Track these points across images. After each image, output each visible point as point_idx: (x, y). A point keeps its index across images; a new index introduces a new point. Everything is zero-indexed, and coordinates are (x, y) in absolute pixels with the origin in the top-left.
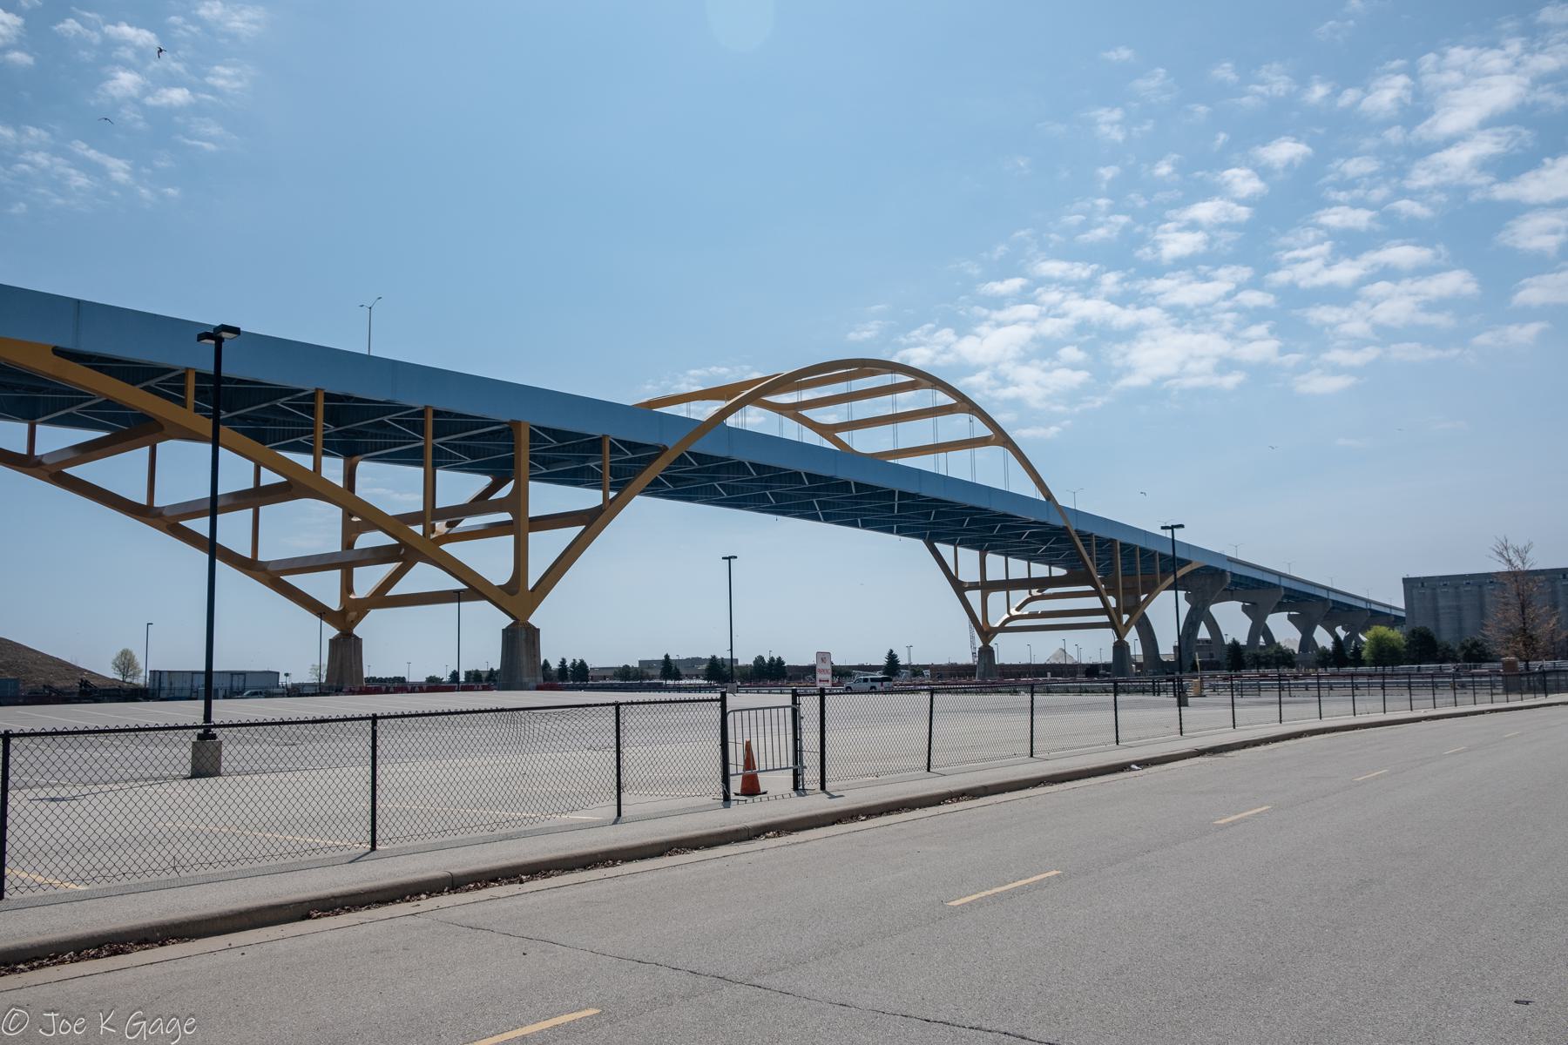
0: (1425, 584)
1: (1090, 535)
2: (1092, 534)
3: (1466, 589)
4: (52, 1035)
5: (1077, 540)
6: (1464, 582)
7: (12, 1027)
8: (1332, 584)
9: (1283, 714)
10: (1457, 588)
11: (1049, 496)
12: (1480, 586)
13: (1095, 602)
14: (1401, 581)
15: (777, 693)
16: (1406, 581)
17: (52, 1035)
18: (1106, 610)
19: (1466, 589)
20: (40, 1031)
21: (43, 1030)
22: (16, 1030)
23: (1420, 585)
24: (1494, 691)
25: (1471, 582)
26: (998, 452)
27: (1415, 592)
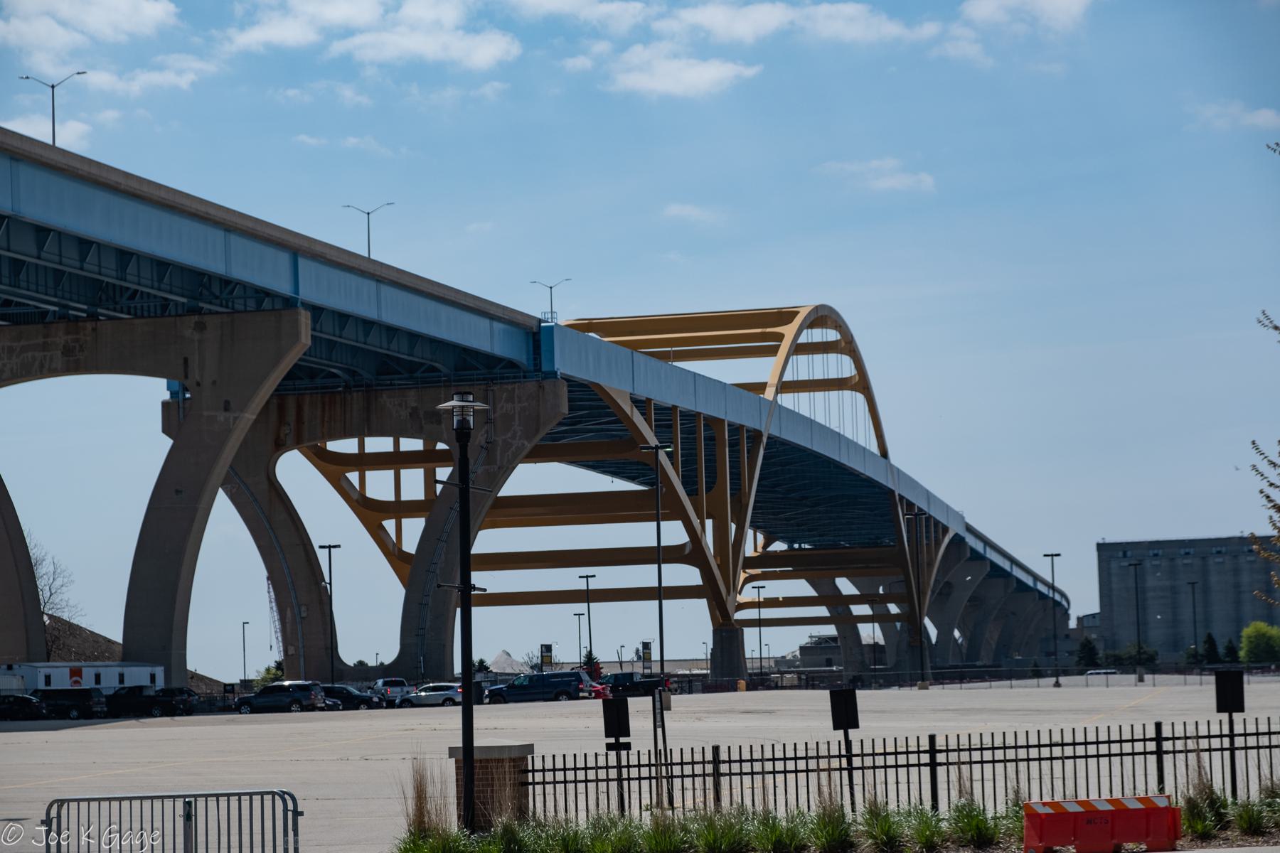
0: (1129, 553)
1: (649, 400)
2: (675, 407)
3: (1186, 561)
4: (41, 845)
5: (638, 419)
6: (1182, 551)
7: (10, 838)
8: (696, 408)
9: (1123, 733)
10: (1172, 559)
11: (884, 454)
12: (1203, 558)
13: (674, 534)
14: (1095, 548)
15: (986, 688)
16: (1102, 548)
17: (41, 845)
18: (691, 554)
19: (1186, 561)
20: (33, 841)
21: (36, 841)
22: (13, 841)
23: (1121, 554)
24: (530, 768)
25: (1192, 551)
26: (860, 398)
27: (1114, 565)
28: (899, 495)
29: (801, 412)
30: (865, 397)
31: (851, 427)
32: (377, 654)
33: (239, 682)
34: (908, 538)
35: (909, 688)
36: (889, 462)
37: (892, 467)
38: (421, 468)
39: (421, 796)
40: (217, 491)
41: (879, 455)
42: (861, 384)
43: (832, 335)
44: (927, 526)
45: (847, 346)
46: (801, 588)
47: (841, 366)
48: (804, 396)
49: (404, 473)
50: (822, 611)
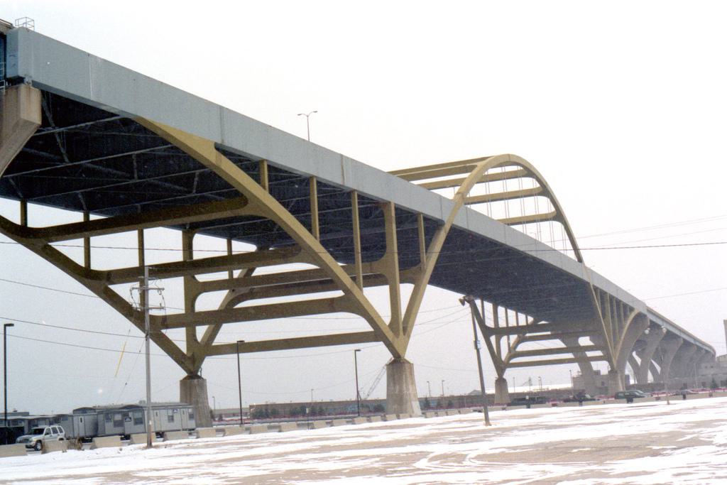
11: (580, 260)
14: (723, 322)
28: (594, 286)
29: (312, 140)
30: (562, 223)
31: (492, 209)
32: (312, 390)
33: (248, 407)
34: (109, 159)
35: (268, 403)
36: (584, 264)
37: (586, 268)
38: (81, 237)
39: (432, 452)
40: (372, 326)
41: (577, 260)
42: (559, 216)
43: (529, 183)
44: (612, 306)
45: (544, 191)
46: (557, 343)
47: (544, 206)
48: (529, 225)
49: (515, 324)
50: (570, 356)
